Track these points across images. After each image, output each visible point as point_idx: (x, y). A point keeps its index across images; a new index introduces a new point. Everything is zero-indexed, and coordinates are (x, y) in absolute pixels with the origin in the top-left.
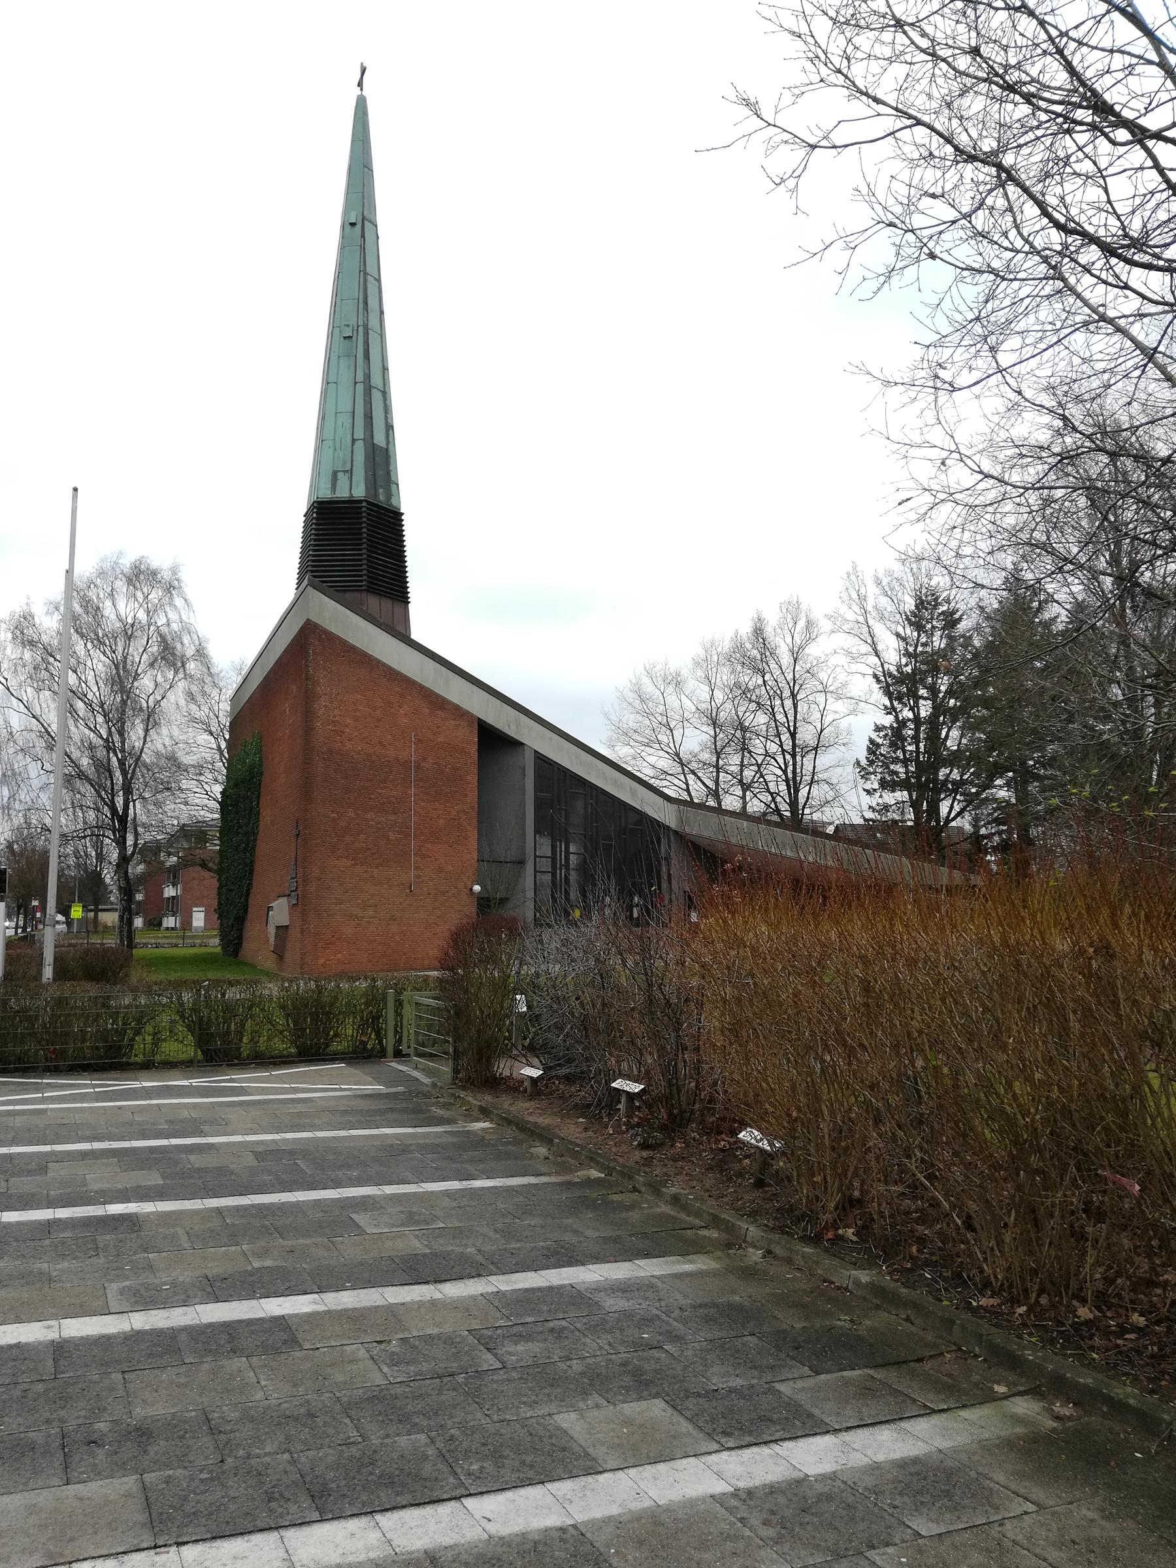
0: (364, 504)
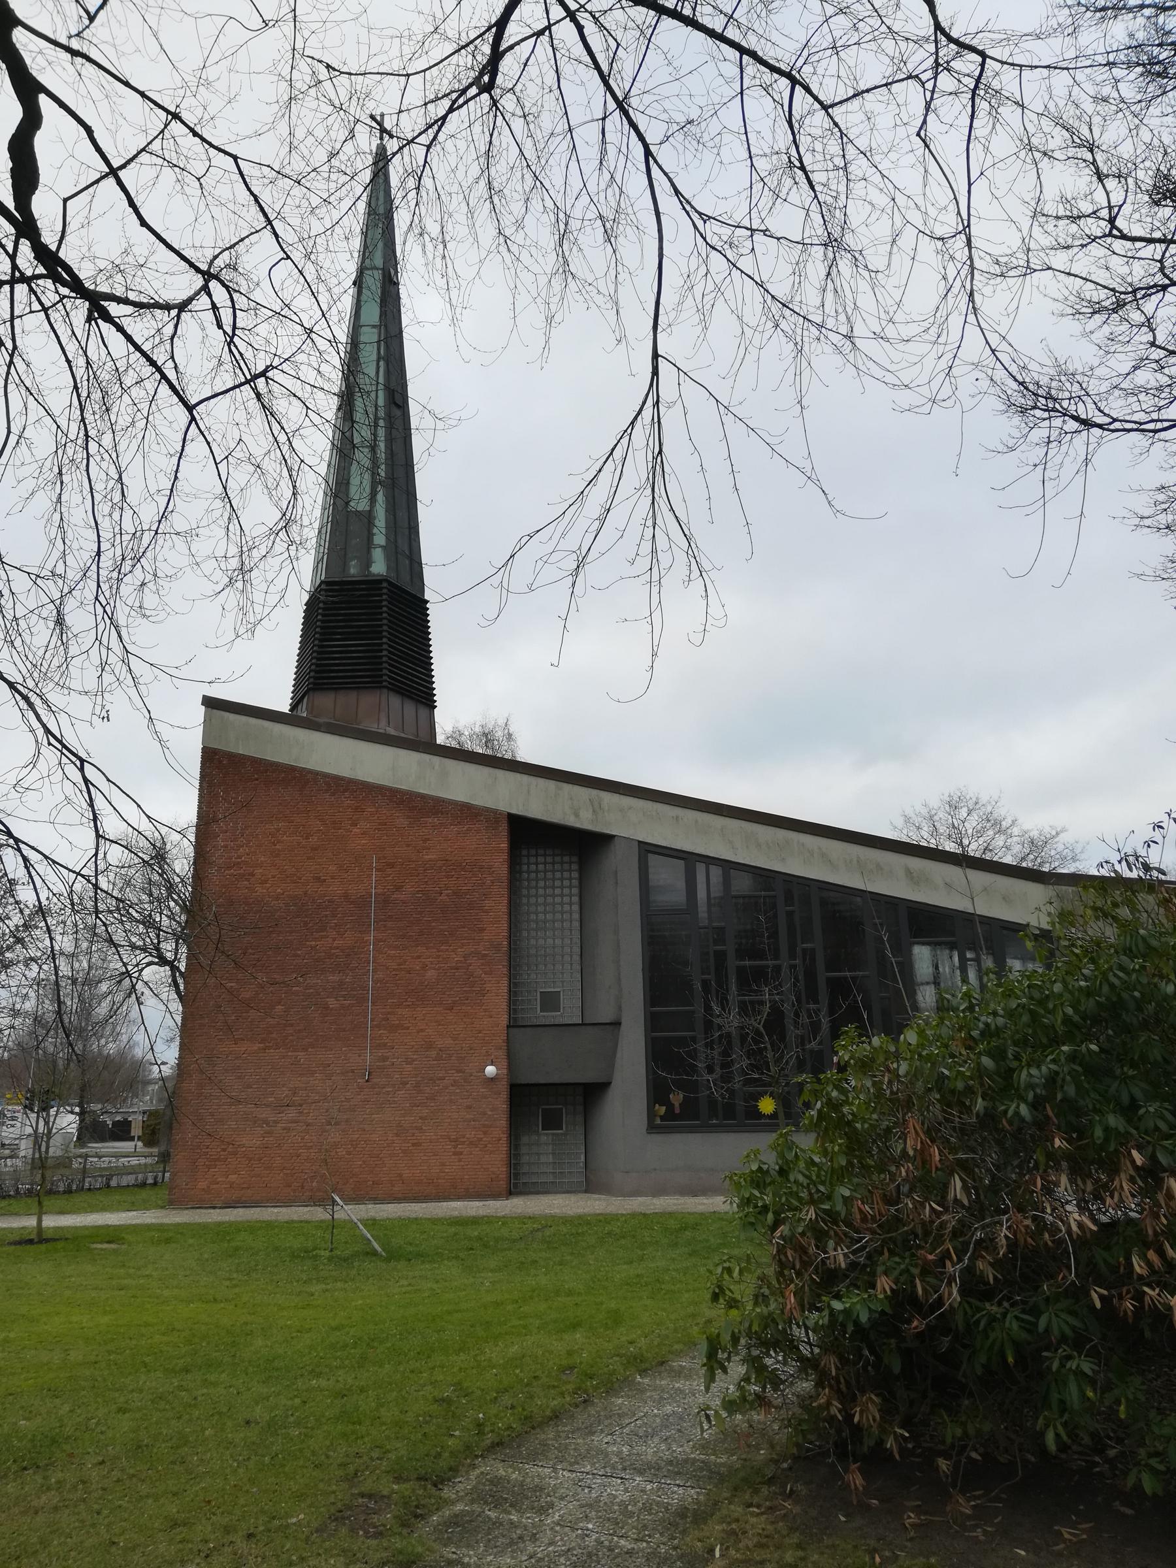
0: (385, 585)
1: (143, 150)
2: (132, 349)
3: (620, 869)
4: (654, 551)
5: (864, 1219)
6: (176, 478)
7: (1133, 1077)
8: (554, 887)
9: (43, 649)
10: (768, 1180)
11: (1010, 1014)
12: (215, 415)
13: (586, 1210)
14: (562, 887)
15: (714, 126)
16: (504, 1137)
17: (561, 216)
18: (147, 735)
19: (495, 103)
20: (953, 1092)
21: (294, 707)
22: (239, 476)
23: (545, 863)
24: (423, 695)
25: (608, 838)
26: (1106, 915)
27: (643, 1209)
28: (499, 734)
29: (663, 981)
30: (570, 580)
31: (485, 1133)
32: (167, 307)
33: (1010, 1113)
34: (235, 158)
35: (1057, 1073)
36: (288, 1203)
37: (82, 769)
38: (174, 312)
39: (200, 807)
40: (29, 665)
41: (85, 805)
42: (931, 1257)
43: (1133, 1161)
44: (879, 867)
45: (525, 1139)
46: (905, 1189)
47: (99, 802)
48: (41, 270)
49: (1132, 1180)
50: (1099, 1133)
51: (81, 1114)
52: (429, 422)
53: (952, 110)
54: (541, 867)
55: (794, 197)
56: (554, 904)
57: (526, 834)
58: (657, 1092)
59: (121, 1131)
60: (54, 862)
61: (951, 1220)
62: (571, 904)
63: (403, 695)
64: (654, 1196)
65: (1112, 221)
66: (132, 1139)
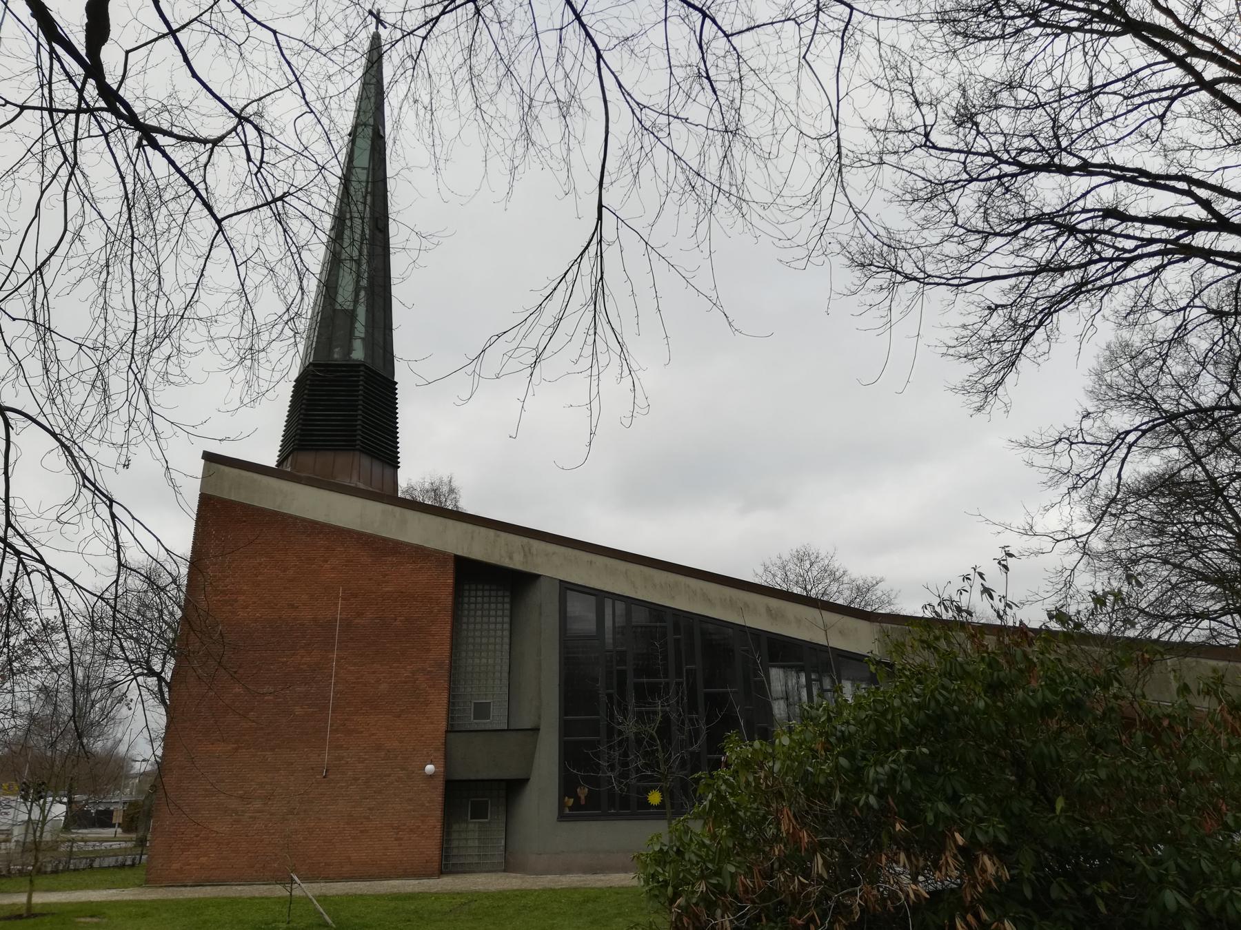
1: (195, 19)
2: (172, 170)
3: (543, 602)
4: (594, 354)
5: (746, 891)
6: (202, 275)
7: (954, 774)
8: (489, 616)
9: (79, 408)
10: (668, 859)
11: (861, 723)
12: (235, 227)
13: (506, 887)
14: (496, 616)
15: (644, 41)
16: (439, 825)
17: (526, 98)
18: (164, 481)
19: (478, 11)
20: (816, 785)
21: (280, 463)
22: (255, 277)
23: (483, 596)
24: (389, 457)
25: (535, 577)
26: (929, 647)
27: (552, 885)
28: (445, 489)
29: (575, 693)
30: (529, 371)
31: (423, 822)
32: (204, 141)
33: (861, 803)
34: (275, 32)
35: (897, 771)
36: (250, 882)
37: (110, 507)
38: (209, 146)
39: (194, 543)
40: (66, 418)
41: (111, 538)
42: (799, 922)
43: (955, 841)
44: (746, 605)
45: (455, 827)
46: (776, 866)
47: (124, 536)
48: (102, 104)
49: (955, 857)
50: (930, 817)
51: (70, 803)
52: (415, 242)
53: (827, 48)
54: (479, 599)
55: (701, 98)
56: (489, 630)
57: (471, 574)
58: (567, 786)
59: (104, 820)
60: (80, 587)
61: (815, 890)
62: (502, 630)
63: (373, 457)
64: (561, 874)
65: (927, 135)
66: (113, 826)
